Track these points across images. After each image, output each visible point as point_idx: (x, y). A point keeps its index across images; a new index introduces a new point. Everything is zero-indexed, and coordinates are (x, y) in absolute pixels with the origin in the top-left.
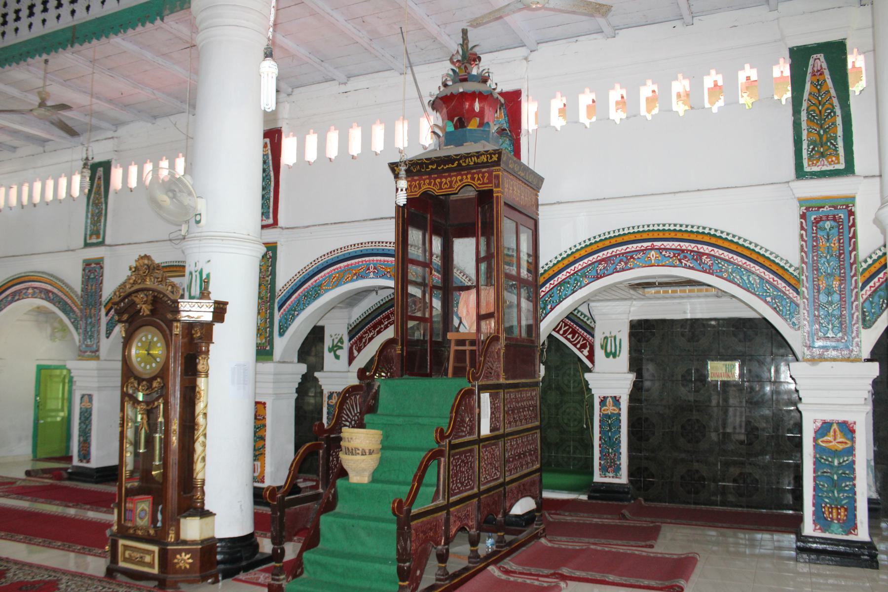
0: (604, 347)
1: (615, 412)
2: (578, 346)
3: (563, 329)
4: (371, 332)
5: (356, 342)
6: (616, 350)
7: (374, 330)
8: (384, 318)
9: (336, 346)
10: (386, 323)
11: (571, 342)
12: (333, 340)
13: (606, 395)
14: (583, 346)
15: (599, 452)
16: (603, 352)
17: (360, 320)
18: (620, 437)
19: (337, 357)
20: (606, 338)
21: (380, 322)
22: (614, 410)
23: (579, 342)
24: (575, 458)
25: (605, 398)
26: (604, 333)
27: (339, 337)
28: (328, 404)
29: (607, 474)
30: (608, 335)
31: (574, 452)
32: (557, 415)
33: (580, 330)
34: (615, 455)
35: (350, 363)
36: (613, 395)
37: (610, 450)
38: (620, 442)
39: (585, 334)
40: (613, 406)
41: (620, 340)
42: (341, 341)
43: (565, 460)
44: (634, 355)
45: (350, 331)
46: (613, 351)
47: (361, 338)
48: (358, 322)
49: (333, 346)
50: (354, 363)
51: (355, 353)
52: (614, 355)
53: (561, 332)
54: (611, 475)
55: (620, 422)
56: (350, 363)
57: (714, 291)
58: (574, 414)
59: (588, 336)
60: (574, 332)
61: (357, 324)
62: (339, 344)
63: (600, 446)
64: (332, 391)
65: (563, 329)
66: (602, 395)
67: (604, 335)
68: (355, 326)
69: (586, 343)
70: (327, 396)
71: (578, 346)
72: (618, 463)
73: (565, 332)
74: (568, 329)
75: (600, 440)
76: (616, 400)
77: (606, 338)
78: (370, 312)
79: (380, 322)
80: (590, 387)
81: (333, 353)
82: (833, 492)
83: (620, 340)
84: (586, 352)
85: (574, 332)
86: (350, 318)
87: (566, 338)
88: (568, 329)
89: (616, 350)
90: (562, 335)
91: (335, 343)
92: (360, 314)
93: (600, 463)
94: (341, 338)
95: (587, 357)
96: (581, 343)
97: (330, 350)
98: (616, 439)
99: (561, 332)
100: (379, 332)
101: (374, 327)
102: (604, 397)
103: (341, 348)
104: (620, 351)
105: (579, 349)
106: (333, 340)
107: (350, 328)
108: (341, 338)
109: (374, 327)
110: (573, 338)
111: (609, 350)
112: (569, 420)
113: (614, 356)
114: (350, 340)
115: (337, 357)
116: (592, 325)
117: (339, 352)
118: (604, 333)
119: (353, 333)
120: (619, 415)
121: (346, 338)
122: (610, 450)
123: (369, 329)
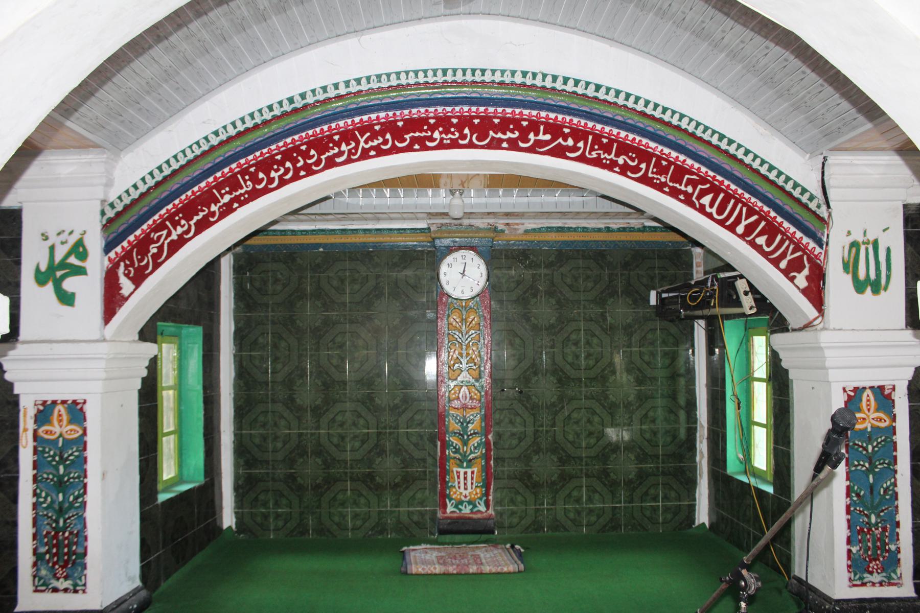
0: (850, 266)
1: (882, 425)
2: (783, 264)
3: (744, 223)
4: (176, 224)
5: (127, 255)
6: (878, 274)
7: (188, 219)
8: (219, 186)
9: (63, 265)
10: (227, 198)
11: (765, 255)
12: (52, 249)
13: (860, 385)
14: (795, 266)
15: (845, 525)
16: (848, 278)
17: (143, 188)
18: (895, 485)
19: (66, 299)
20: (854, 245)
21: (208, 198)
22: (881, 420)
23: (784, 255)
24: (591, 511)
25: (858, 391)
26: (849, 233)
27: (72, 240)
28: (36, 437)
29: (868, 577)
30: (860, 239)
31: (590, 500)
32: (554, 425)
33: (786, 225)
34: (884, 529)
35: (109, 313)
36: (876, 384)
37: (873, 519)
38: (896, 496)
39: (799, 235)
40: (877, 410)
41: (888, 250)
42: (79, 249)
43: (572, 515)
44: (856, 285)
45: (110, 221)
46: (873, 276)
47: (143, 245)
48: (135, 195)
49: (52, 268)
50: (122, 314)
51: (126, 286)
52: (877, 288)
53: (740, 229)
54: (876, 578)
55: (895, 450)
56: (109, 313)
57: (600, 214)
58: (589, 421)
59: (805, 240)
60: (772, 231)
61: (134, 202)
62: (73, 260)
63: (848, 512)
64: (50, 398)
65: (744, 223)
66: (850, 386)
67: (851, 239)
68: (127, 208)
69: (801, 257)
70: (32, 412)
71: (783, 264)
72: (893, 547)
73: (749, 229)
74: (757, 223)
75: (848, 495)
76: (884, 397)
77: (854, 245)
78: (175, 166)
79: (208, 198)
80: (784, 364)
81: (50, 286)
82: (868, 517)
83: (888, 250)
84: (801, 279)
85: (772, 231)
86: (109, 184)
87: (752, 244)
88: (757, 223)
89: (878, 274)
90: (743, 237)
91: (58, 257)
92: (144, 173)
93: (849, 551)
94: (80, 243)
95: (805, 292)
96: (789, 257)
97: (41, 278)
98: (886, 491)
99: (740, 229)
100: (203, 225)
101: (188, 210)
102: (856, 390)
103: (81, 271)
104: (888, 277)
105: (786, 272)
106: (52, 249)
107: (111, 214)
108: (80, 243)
109: (188, 210)
110: (769, 243)
111: (862, 275)
112: (578, 435)
113: (876, 289)
114: (108, 249)
115: (66, 299)
116: (823, 212)
117: (70, 284)
118: (849, 233)
119: (120, 226)
120: (893, 431)
121: (95, 243)
122: (873, 519)
123: (171, 217)
